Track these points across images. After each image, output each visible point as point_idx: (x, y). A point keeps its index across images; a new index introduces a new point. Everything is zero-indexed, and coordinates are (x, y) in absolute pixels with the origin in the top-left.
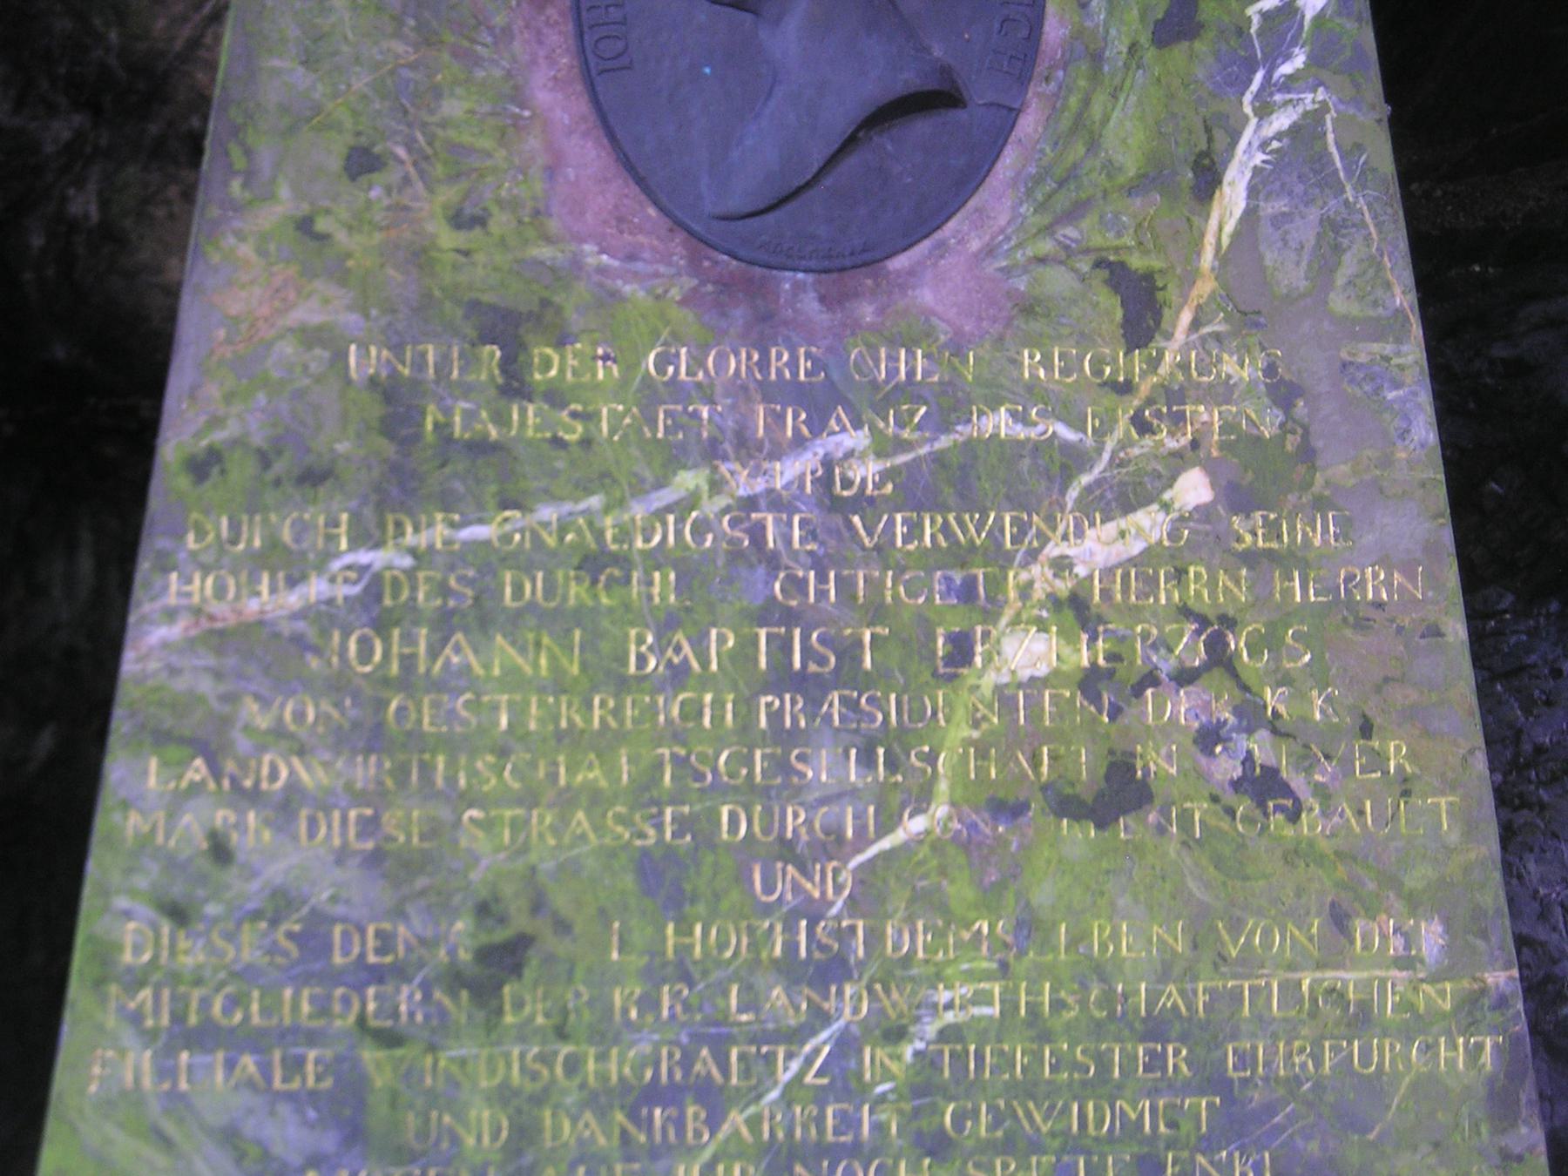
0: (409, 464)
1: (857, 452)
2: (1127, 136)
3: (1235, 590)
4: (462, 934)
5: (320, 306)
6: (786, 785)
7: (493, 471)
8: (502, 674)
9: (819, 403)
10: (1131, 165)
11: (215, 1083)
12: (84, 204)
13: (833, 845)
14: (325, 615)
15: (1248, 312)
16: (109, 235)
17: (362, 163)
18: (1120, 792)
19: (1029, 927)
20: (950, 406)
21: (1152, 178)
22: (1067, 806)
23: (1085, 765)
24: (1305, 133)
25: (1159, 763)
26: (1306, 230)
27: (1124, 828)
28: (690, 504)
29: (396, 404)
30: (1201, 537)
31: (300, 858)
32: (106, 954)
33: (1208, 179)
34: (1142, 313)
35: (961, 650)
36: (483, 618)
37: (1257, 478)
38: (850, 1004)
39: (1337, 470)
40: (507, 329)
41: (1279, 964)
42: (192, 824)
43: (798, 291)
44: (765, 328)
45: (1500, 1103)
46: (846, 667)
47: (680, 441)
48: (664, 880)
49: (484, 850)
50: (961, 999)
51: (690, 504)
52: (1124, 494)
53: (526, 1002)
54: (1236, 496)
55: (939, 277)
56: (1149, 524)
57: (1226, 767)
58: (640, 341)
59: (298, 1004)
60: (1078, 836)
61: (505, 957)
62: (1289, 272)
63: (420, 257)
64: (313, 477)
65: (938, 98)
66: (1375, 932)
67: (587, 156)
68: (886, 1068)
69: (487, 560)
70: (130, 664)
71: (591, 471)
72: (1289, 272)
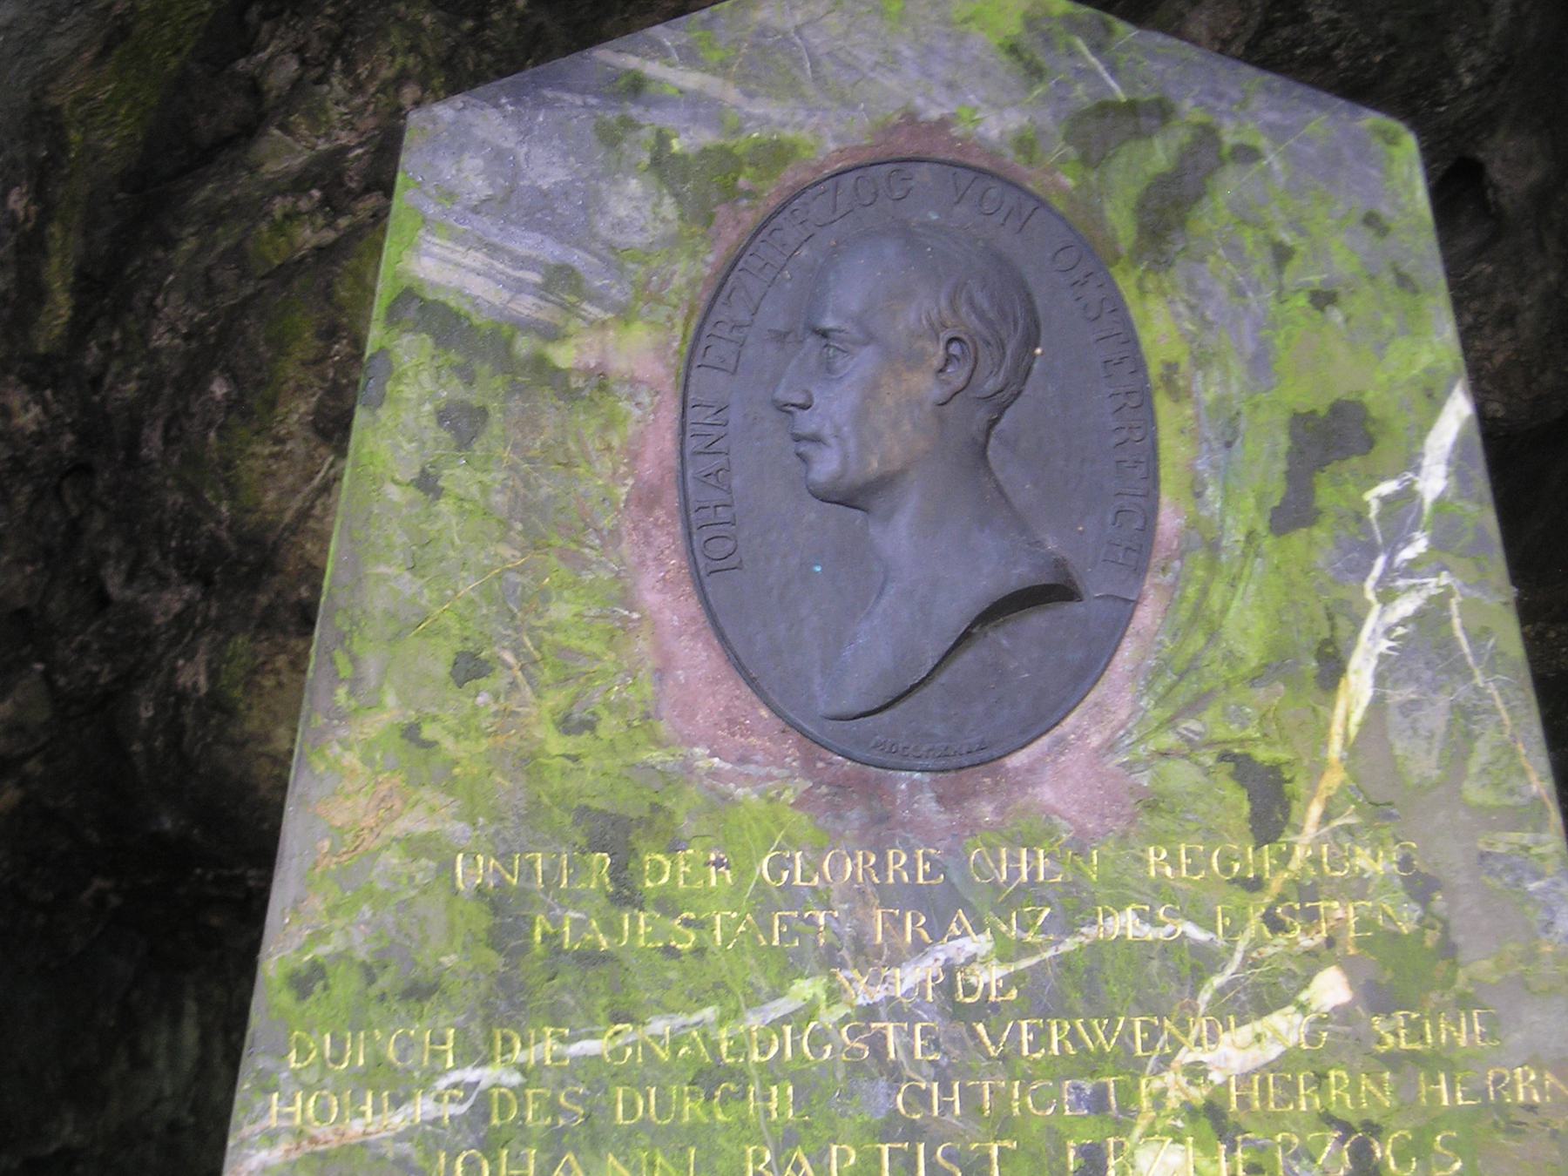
0: (518, 975)
1: (979, 956)
2: (1247, 624)
7: (605, 984)
9: (939, 906)
12: (194, 675)
15: (1380, 805)
16: (218, 705)
17: (469, 668)
20: (1075, 907)
24: (1430, 618)
26: (1435, 717)
29: (504, 915)
30: (1341, 1039)
33: (1332, 667)
34: (1270, 810)
37: (1396, 976)
40: (616, 835)
43: (916, 793)
44: (881, 830)
47: (789, 941)
52: (1260, 997)
54: (1377, 997)
55: (1060, 773)
56: (1285, 1028)
58: (753, 843)
62: (1420, 762)
65: (1054, 591)
67: (697, 658)
72: (1420, 762)
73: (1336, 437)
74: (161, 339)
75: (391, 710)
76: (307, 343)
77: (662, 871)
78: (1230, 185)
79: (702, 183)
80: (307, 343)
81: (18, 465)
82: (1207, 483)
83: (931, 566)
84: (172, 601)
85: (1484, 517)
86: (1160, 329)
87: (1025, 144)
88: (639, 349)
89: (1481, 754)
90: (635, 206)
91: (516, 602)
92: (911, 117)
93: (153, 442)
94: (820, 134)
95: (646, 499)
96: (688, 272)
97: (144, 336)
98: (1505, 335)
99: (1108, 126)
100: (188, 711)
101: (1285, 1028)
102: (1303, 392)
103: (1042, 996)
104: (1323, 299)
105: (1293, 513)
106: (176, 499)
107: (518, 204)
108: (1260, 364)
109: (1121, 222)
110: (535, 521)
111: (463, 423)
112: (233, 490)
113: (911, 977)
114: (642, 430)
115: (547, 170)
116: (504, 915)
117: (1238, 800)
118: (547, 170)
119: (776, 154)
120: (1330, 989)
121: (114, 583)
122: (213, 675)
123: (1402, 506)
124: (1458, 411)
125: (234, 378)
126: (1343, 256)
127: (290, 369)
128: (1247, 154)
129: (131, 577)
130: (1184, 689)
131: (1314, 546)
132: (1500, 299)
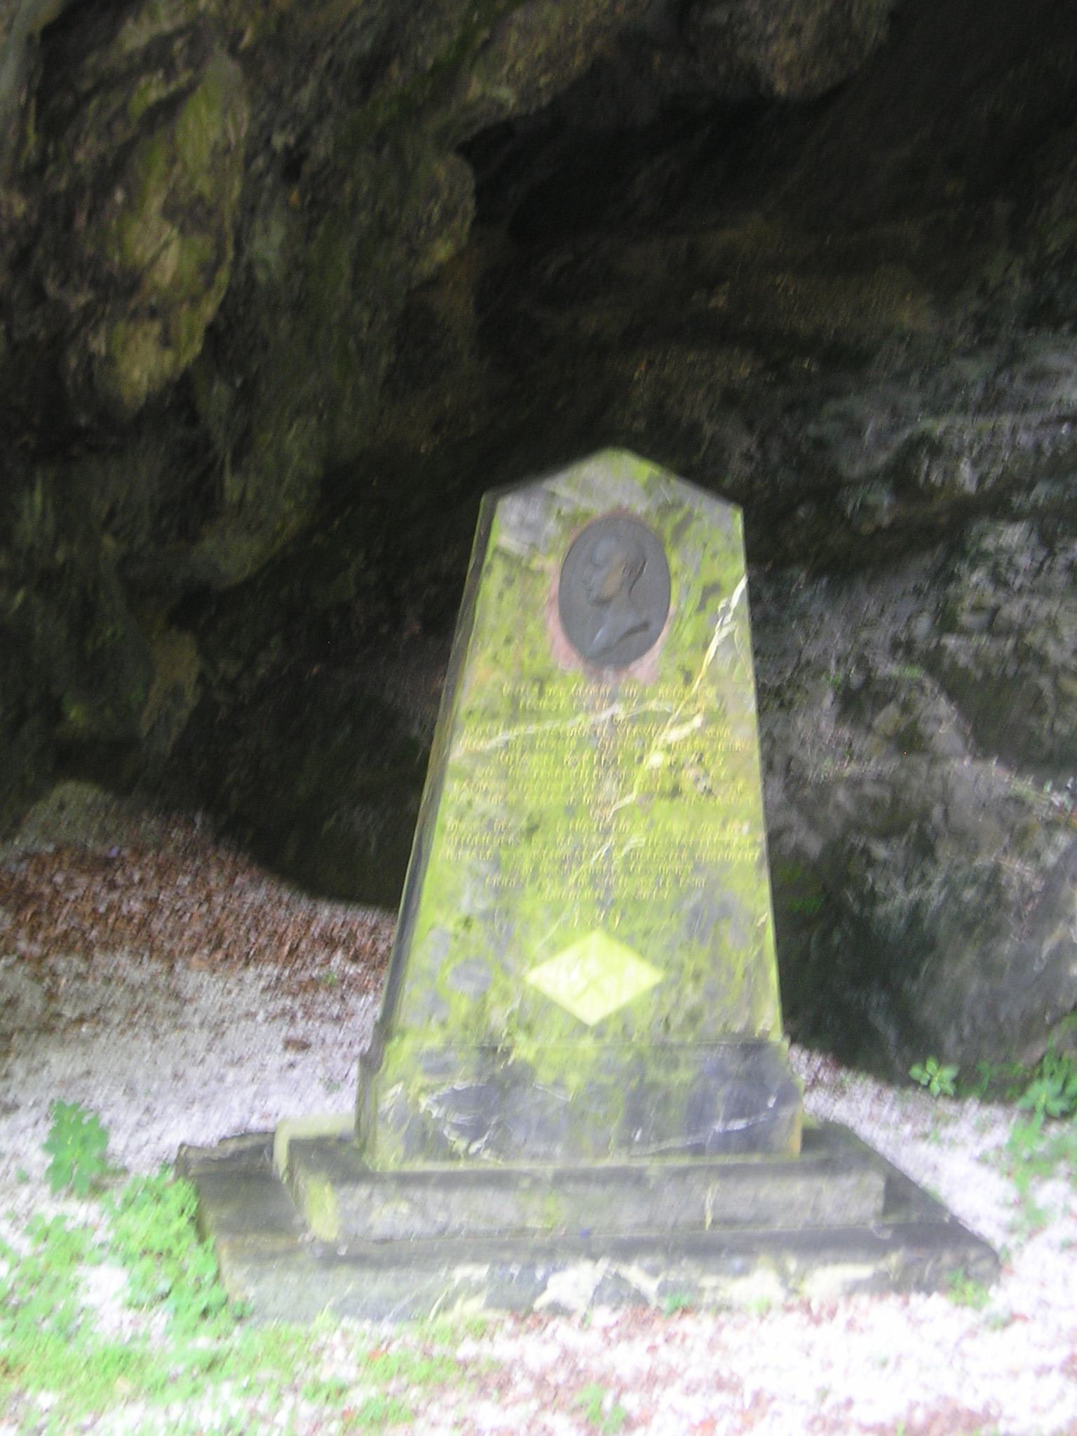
0: (516, 712)
1: (620, 711)
2: (688, 635)
3: (705, 745)
4: (524, 823)
5: (497, 675)
6: (800, 668)
7: (535, 715)
8: (536, 763)
9: (612, 699)
10: (688, 643)
11: (468, 856)
12: (98, 345)
13: (608, 804)
14: (495, 750)
15: (713, 678)
16: (110, 359)
17: (508, 641)
18: (676, 792)
19: (652, 824)
20: (642, 701)
21: (693, 645)
22: (662, 794)
23: (668, 786)
24: (730, 637)
25: (686, 786)
26: (729, 657)
27: (676, 802)
28: (581, 723)
29: (514, 700)
30: (700, 732)
31: (490, 805)
32: (443, 828)
33: (706, 646)
34: (688, 679)
35: (641, 759)
36: (532, 749)
37: (712, 718)
38: (611, 840)
39: (732, 716)
40: (541, 681)
41: (710, 833)
42: (464, 797)
43: (608, 673)
44: (600, 681)
45: (759, 866)
46: (613, 760)
47: (577, 704)
48: (570, 811)
49: (530, 803)
50: (637, 839)
51: (581, 723)
52: (682, 721)
53: (538, 838)
54: (708, 722)
55: (642, 668)
56: (686, 730)
57: (700, 787)
58: (570, 680)
59: (486, 838)
60: (665, 804)
61: (532, 830)
62: (723, 668)
63: (521, 664)
64: (495, 716)
65: (645, 626)
66: (733, 827)
67: (561, 640)
68: (619, 856)
69: (533, 737)
70: (451, 760)
71: (557, 714)
72: (723, 668)
73: (713, 590)
74: (80, 156)
75: (489, 651)
76: (160, 166)
77: (549, 690)
78: (694, 526)
79: (570, 522)
80: (160, 166)
81: (12, 231)
82: (681, 600)
83: (619, 619)
84: (80, 300)
85: (745, 610)
86: (675, 562)
87: (648, 514)
88: (550, 564)
89: (739, 666)
90: (552, 527)
91: (520, 626)
92: (619, 507)
93: (81, 220)
94: (598, 508)
95: (551, 602)
96: (564, 545)
97: (71, 154)
98: (793, 41)
99: (666, 509)
100: (96, 365)
101: (686, 730)
102: (706, 578)
103: (633, 720)
104: (714, 555)
105: (701, 607)
106: (89, 250)
107: (524, 525)
108: (697, 572)
109: (668, 533)
110: (526, 605)
111: (509, 581)
112: (121, 248)
113: (605, 715)
114: (550, 586)
115: (533, 516)
116: (514, 700)
117: (681, 680)
118: (533, 516)
119: (587, 515)
120: (697, 721)
121: (51, 287)
122: (108, 344)
123: (726, 610)
124: (743, 584)
125: (128, 191)
126: (720, 543)
127: (153, 183)
128: (699, 519)
129: (63, 285)
130: (672, 650)
131: (706, 616)
132: (792, 19)
